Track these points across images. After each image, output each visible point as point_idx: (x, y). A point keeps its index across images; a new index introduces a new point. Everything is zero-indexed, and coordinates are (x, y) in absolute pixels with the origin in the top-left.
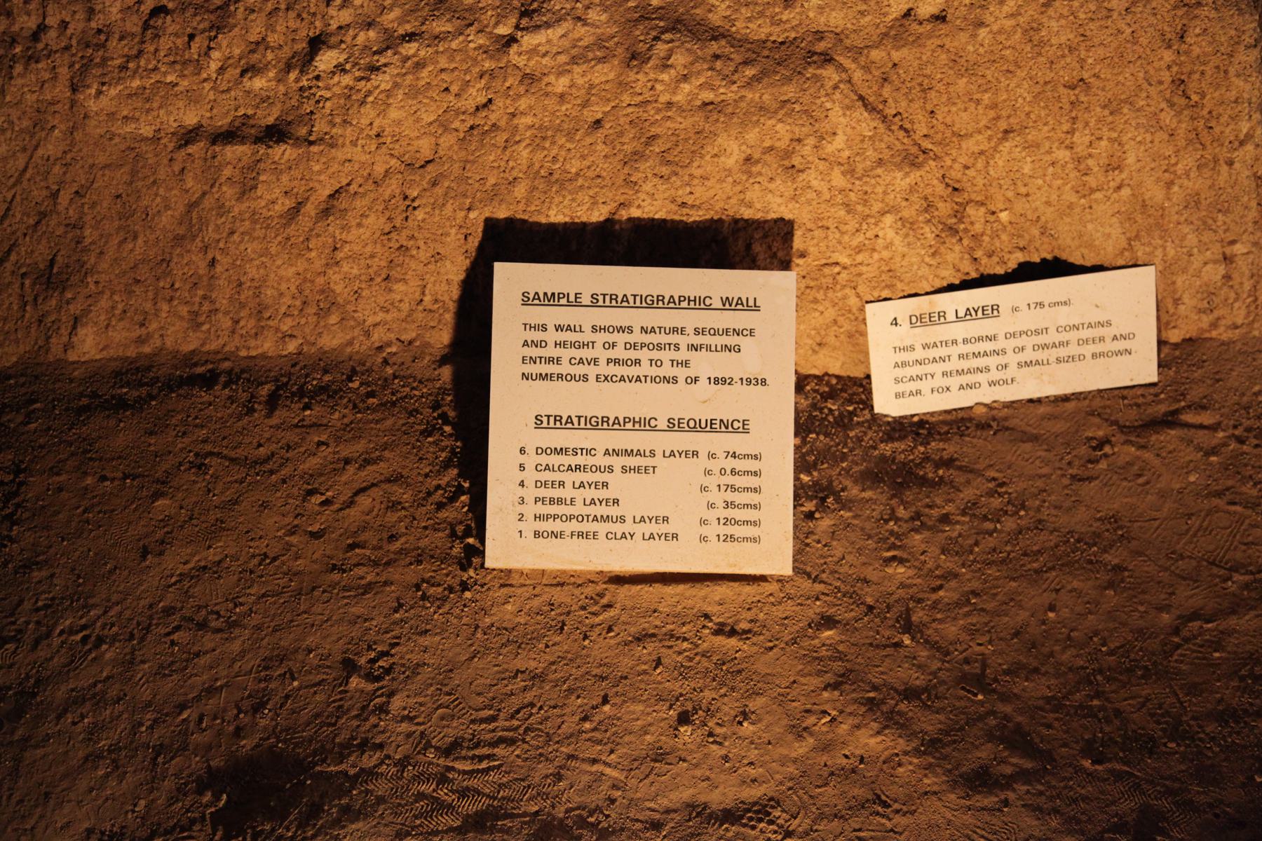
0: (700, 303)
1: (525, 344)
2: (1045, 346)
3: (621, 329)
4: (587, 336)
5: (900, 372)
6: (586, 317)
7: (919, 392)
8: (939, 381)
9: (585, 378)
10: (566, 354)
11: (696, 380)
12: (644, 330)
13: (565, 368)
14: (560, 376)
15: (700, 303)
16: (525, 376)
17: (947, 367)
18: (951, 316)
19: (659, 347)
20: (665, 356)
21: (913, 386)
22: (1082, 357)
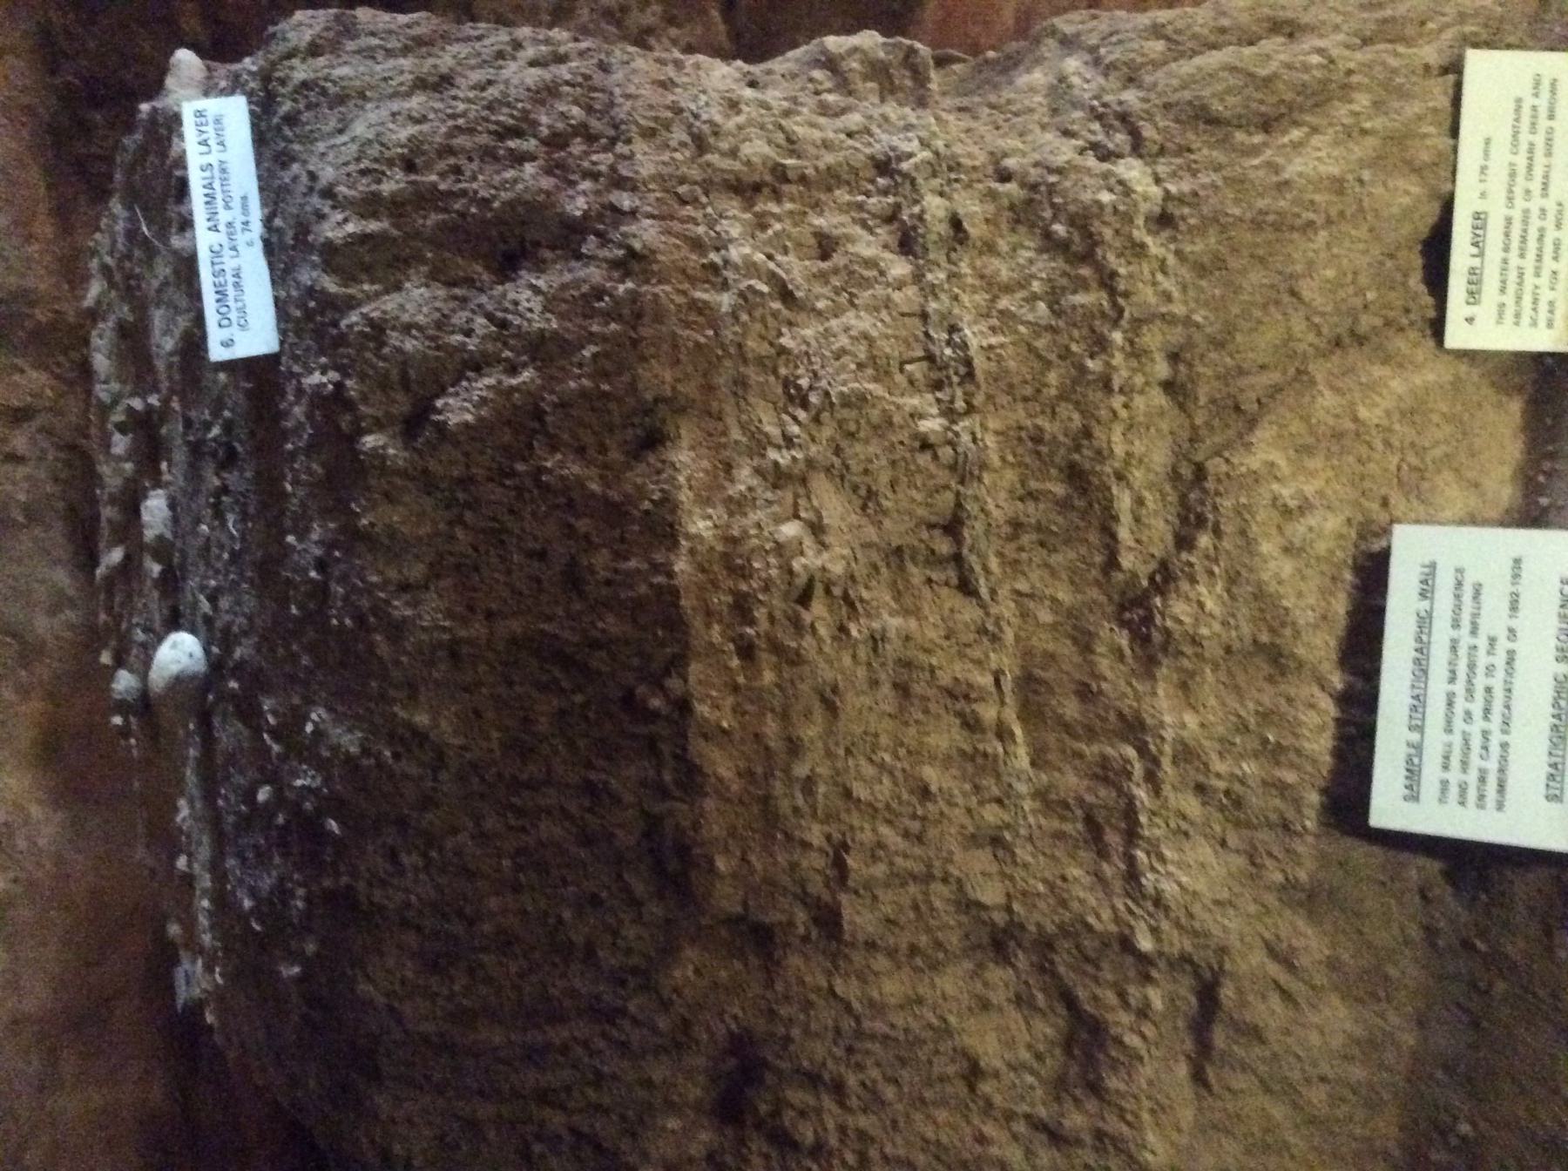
0: (1425, 622)
1: (1462, 803)
2: (1530, 168)
3: (1450, 704)
4: (1457, 739)
5: (1525, 320)
6: (1435, 739)
7: (1551, 303)
8: (1544, 280)
9: (1504, 746)
10: (1475, 761)
11: (1512, 631)
12: (1452, 680)
13: (1492, 765)
14: (1502, 770)
15: (1425, 622)
16: (1500, 806)
17: (1529, 272)
18: (1476, 262)
19: (1472, 666)
20: (1482, 660)
21: (1543, 307)
22: (1550, 131)
